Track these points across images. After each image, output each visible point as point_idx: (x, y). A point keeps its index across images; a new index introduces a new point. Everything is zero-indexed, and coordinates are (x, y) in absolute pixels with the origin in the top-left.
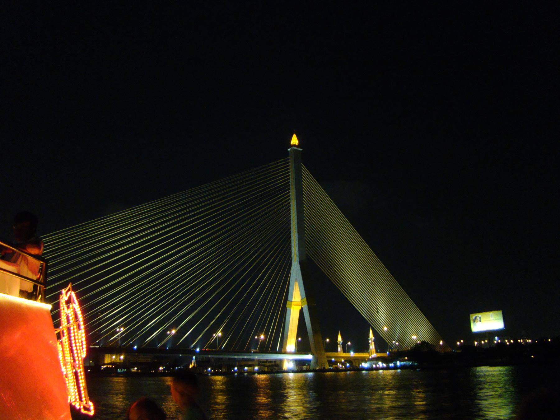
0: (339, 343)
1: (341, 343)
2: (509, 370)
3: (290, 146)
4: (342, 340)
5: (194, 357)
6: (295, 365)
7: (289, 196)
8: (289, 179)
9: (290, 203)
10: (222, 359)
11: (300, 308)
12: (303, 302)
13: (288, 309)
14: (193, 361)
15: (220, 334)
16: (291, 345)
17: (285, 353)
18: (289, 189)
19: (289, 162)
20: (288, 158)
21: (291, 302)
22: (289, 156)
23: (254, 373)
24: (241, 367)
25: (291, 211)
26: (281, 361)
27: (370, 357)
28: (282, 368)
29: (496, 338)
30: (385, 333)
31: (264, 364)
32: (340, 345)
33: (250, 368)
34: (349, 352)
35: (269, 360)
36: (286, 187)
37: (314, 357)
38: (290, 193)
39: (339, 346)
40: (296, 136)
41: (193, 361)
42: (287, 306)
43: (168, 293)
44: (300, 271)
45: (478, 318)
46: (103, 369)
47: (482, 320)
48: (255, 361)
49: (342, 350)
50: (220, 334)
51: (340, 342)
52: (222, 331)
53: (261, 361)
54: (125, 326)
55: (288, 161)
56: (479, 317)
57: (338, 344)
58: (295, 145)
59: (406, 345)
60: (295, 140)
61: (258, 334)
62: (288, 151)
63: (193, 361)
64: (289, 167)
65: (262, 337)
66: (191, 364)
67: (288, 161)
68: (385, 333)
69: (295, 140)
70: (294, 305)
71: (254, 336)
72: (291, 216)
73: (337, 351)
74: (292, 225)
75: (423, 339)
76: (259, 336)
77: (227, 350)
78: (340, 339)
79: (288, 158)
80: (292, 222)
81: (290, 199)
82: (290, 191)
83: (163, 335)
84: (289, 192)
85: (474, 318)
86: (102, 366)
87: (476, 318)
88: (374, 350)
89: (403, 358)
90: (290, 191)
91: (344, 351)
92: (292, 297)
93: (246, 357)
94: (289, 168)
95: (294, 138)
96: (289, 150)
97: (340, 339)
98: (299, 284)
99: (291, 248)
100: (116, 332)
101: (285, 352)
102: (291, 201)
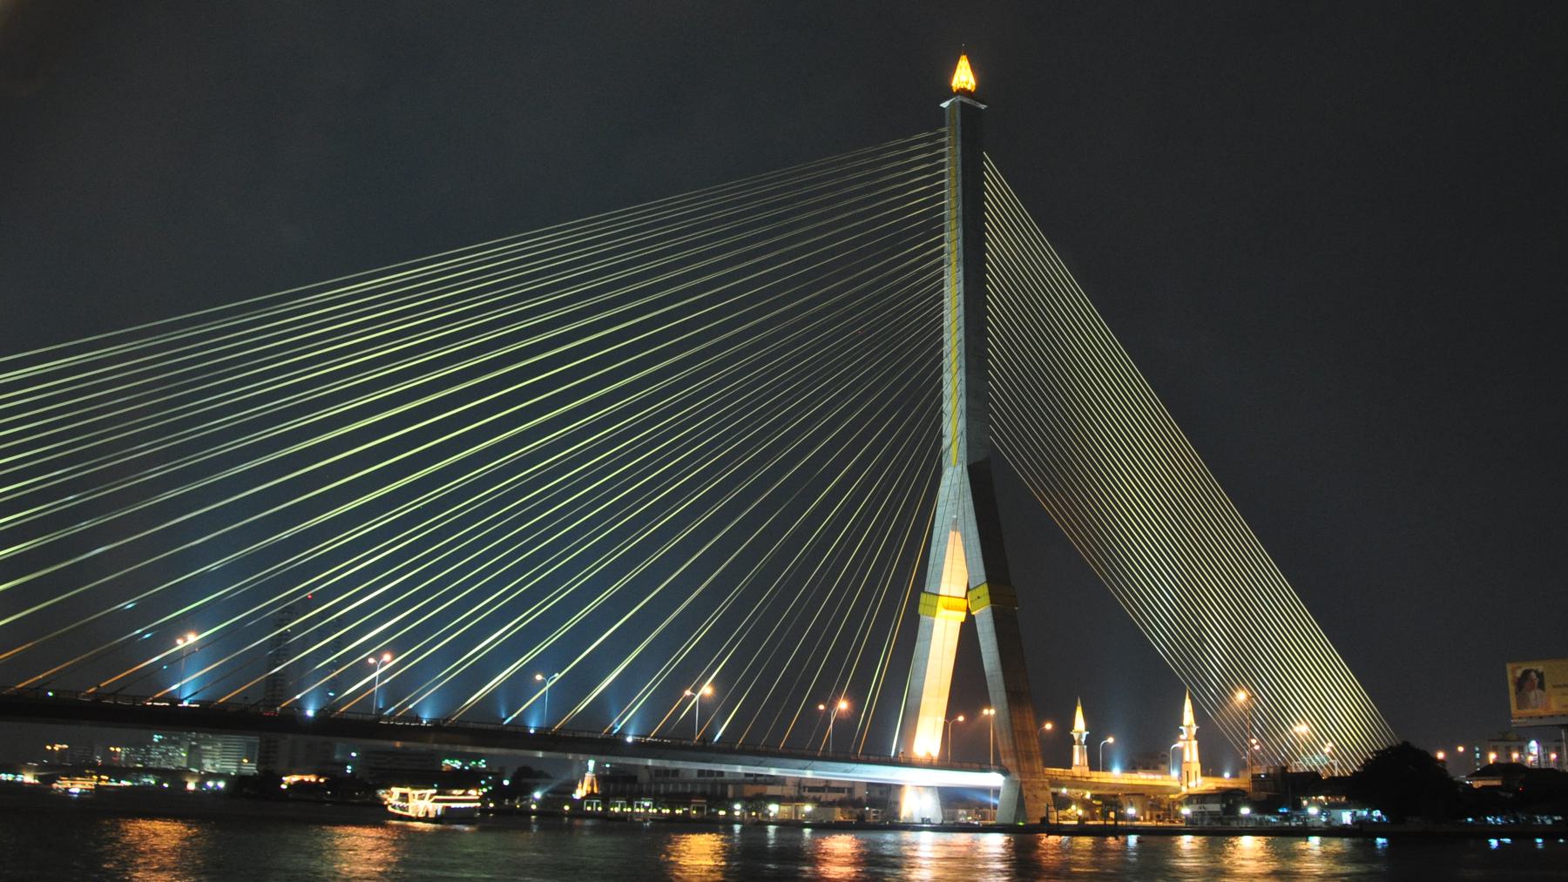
0: (1076, 737)
1: (1083, 740)
2: (188, 839)
3: (948, 93)
4: (1086, 730)
5: (591, 764)
6: (941, 805)
7: (941, 252)
8: (942, 197)
9: (942, 274)
10: (676, 772)
11: (962, 616)
12: (979, 597)
13: (923, 618)
14: (589, 776)
15: (707, 690)
16: (928, 737)
17: (910, 763)
18: (942, 230)
19: (942, 145)
20: (942, 130)
21: (935, 597)
22: (944, 126)
23: (800, 825)
24: (757, 801)
25: (946, 300)
26: (897, 788)
27: (1184, 790)
28: (896, 815)
29: (1533, 744)
30: (1304, 720)
31: (818, 795)
32: (1080, 744)
33: (785, 808)
34: (1106, 768)
35: (833, 785)
36: (934, 225)
37: (1010, 782)
38: (945, 244)
39: (1076, 748)
40: (967, 62)
41: (589, 776)
42: (921, 610)
43: (513, 549)
44: (969, 497)
45: (1533, 675)
46: (290, 786)
47: (1548, 685)
48: (789, 782)
49: (1086, 764)
50: (707, 690)
51: (1081, 737)
52: (714, 683)
53: (809, 784)
54: (396, 648)
55: (942, 140)
56: (1536, 672)
57: (1073, 742)
58: (963, 92)
59: (1285, 753)
60: (964, 76)
61: (826, 692)
62: (944, 109)
63: (587, 774)
64: (942, 161)
65: (843, 705)
66: (580, 785)
67: (942, 140)
68: (1304, 720)
69: (964, 76)
70: (947, 608)
71: (814, 700)
72: (945, 318)
73: (1068, 763)
74: (946, 348)
75: (1376, 745)
76: (831, 705)
77: (728, 750)
78: (1080, 724)
79: (942, 130)
80: (946, 336)
81: (941, 263)
82: (943, 237)
83: (519, 687)
84: (941, 241)
85: (1519, 673)
86: (284, 778)
87: (1526, 673)
88: (1196, 767)
89: (613, 766)
90: (943, 237)
91: (1094, 765)
92: (939, 581)
93: (773, 772)
94: (944, 163)
95: (963, 68)
96: (945, 105)
97: (1080, 724)
98: (965, 538)
99: (940, 420)
100: (365, 669)
101: (907, 760)
102: (946, 270)
